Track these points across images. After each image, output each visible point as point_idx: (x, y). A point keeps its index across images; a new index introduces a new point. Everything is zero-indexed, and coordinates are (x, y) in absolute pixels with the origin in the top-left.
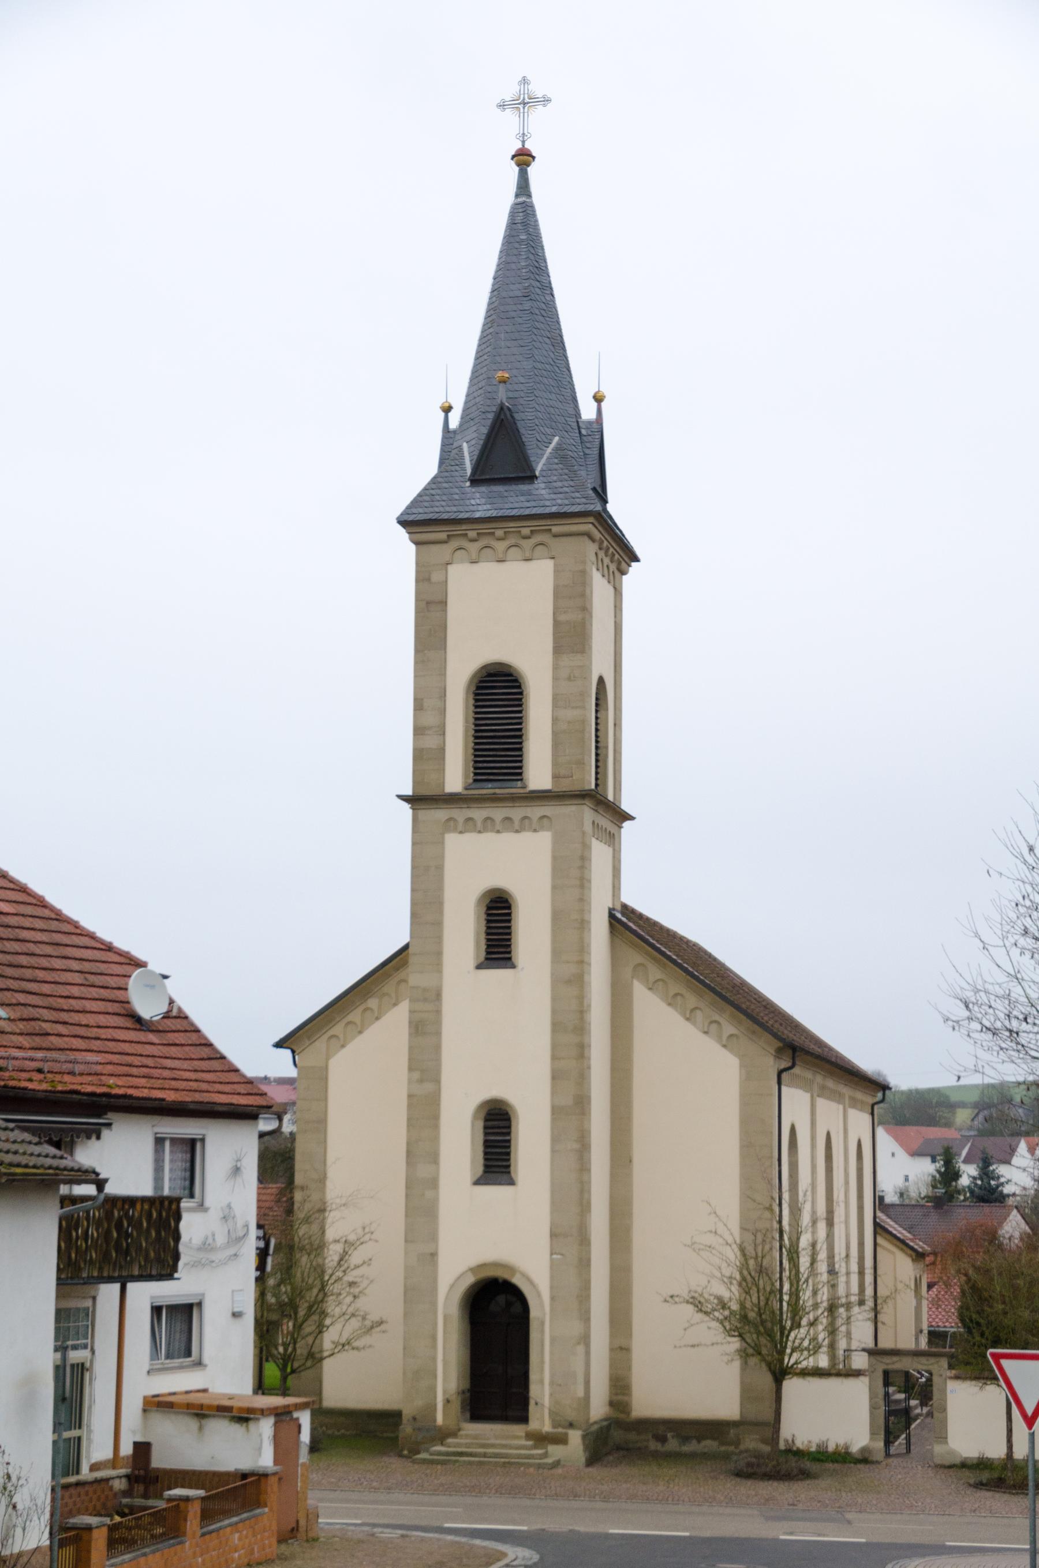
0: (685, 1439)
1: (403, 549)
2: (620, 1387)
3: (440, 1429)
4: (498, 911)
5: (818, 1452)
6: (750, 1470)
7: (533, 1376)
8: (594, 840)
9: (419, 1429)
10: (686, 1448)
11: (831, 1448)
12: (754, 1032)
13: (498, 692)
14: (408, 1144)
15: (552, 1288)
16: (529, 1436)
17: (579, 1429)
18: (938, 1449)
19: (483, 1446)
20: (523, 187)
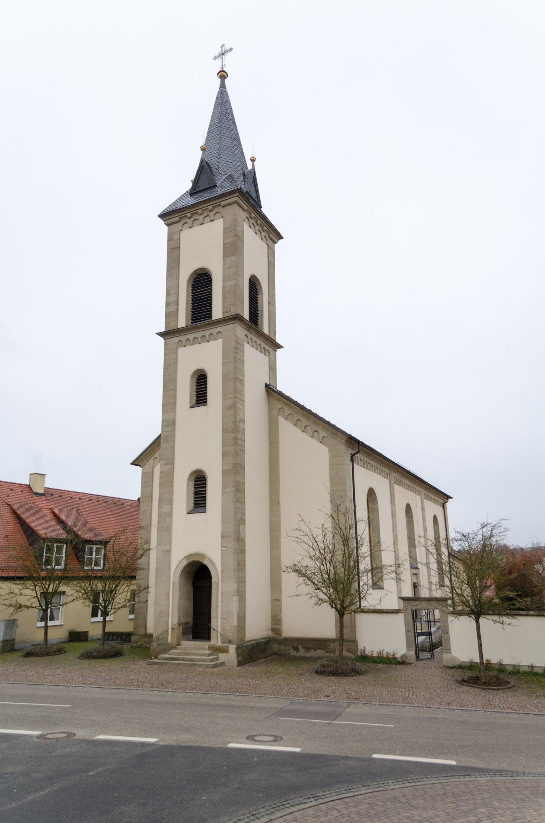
0: (308, 649)
1: (162, 228)
2: (276, 620)
3: (168, 644)
4: (201, 380)
5: (378, 657)
6: (323, 669)
7: (213, 614)
8: (246, 344)
9: (159, 645)
10: (309, 655)
11: (385, 655)
12: (334, 434)
13: (201, 281)
14: (159, 496)
15: (222, 565)
16: (210, 648)
17: (234, 644)
18: (445, 656)
19: (186, 654)
20: (223, 85)
